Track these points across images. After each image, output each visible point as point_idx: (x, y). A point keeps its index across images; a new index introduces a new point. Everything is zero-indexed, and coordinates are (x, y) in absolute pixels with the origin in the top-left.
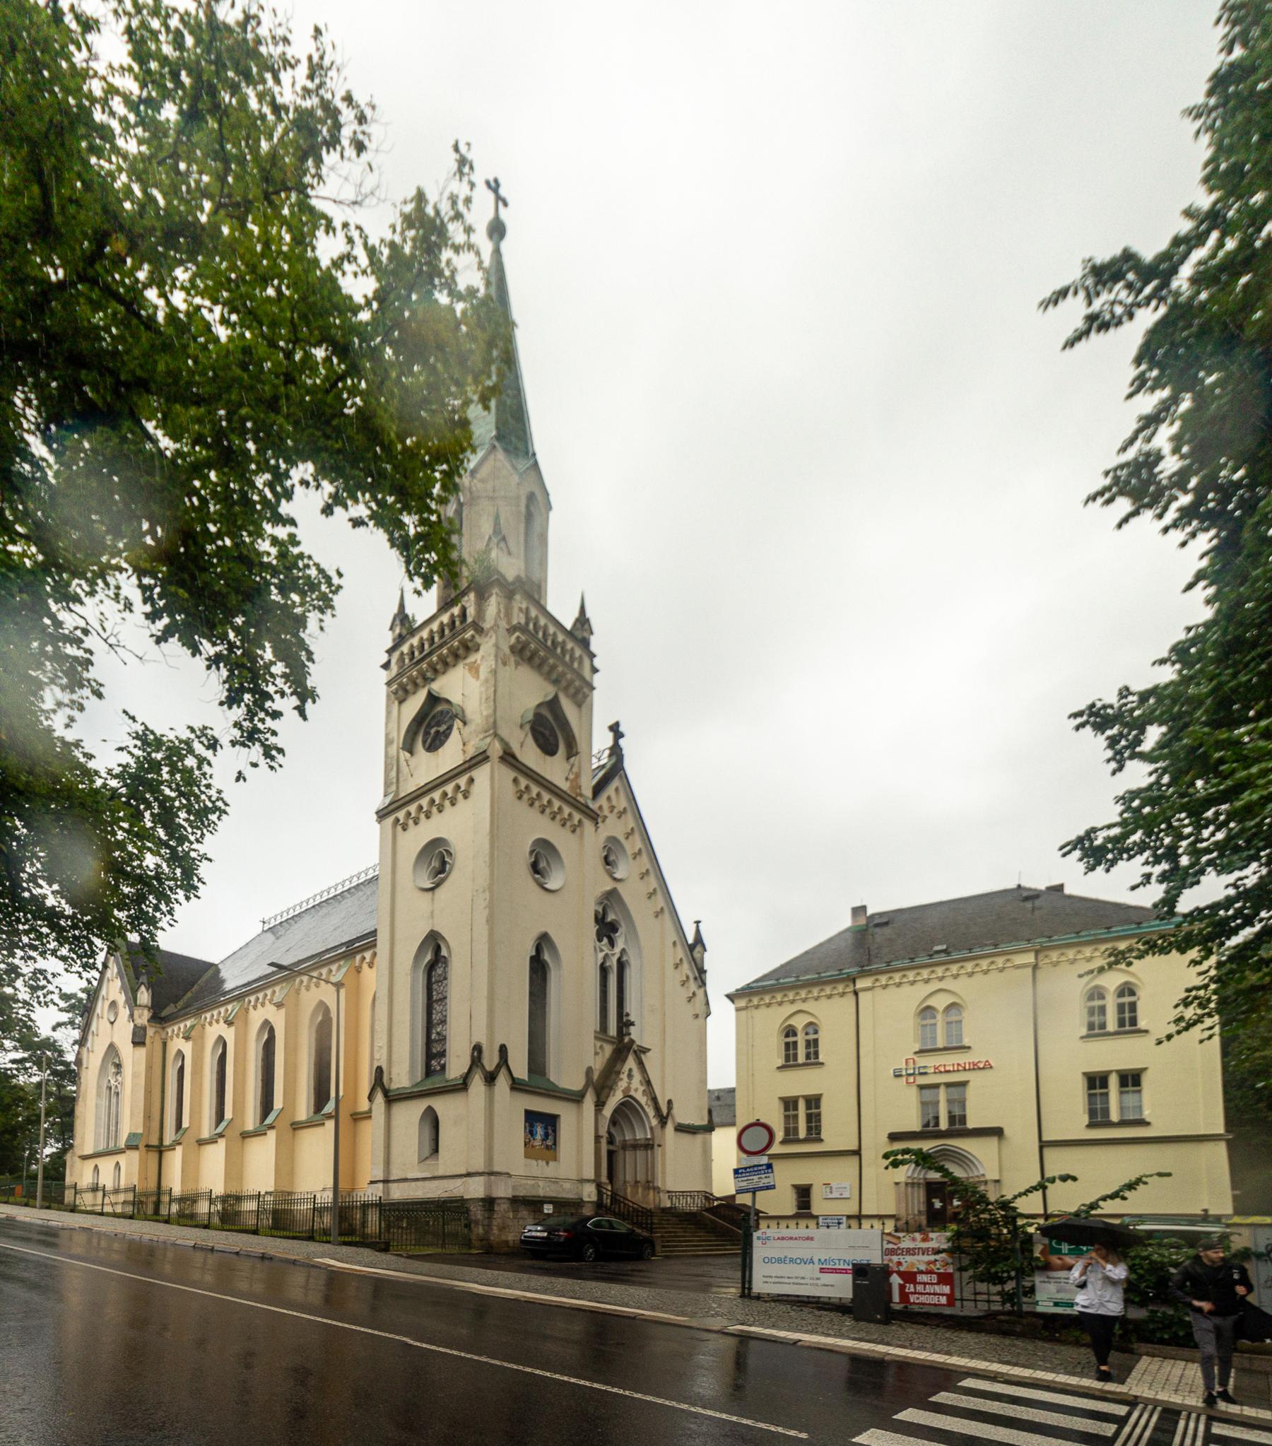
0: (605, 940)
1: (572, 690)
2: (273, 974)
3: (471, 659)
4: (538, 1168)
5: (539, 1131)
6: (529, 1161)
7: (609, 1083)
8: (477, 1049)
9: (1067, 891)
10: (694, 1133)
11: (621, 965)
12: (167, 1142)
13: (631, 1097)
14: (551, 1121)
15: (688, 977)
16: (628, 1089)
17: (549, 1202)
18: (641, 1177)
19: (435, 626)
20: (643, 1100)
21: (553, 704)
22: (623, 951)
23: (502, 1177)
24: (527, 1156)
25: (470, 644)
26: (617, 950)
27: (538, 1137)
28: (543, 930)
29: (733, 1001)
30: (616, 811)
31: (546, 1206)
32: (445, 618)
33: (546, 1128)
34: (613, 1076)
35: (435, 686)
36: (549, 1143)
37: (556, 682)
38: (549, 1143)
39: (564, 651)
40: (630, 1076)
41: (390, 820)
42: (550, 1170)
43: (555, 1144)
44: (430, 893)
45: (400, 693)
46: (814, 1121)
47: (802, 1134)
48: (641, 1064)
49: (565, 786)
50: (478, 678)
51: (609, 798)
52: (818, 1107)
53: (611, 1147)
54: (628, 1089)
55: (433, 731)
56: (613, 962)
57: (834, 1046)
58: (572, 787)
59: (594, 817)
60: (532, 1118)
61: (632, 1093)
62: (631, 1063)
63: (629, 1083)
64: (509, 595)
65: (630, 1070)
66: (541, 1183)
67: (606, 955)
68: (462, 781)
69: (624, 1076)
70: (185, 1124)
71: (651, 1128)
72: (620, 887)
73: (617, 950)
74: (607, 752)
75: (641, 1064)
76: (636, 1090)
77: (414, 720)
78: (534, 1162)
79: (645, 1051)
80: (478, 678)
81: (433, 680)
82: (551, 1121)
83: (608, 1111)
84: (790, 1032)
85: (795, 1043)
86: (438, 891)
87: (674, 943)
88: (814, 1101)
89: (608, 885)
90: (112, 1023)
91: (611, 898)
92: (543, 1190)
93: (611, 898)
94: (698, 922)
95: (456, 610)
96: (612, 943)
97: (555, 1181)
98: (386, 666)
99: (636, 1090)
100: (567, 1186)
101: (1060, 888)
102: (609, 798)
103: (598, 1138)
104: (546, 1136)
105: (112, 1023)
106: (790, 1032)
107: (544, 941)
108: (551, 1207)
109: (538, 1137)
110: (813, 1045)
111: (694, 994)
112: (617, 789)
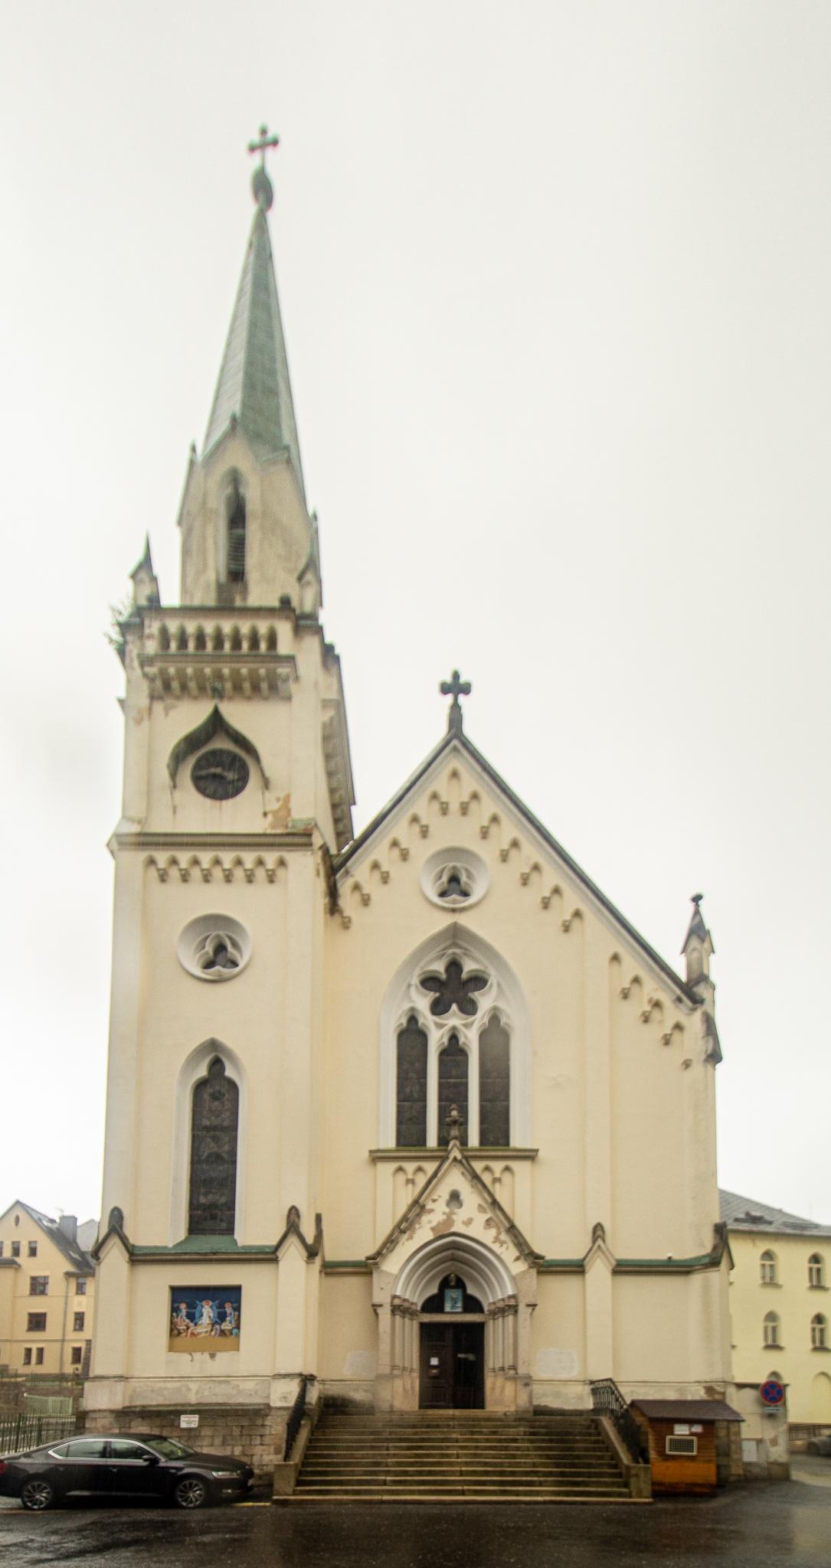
2: (439, 1168)
6: (174, 1355)
8: (293, 1213)
9: (123, 695)
10: (688, 1273)
17: (192, 1412)
18: (509, 1362)
20: (487, 1236)
23: (105, 1383)
27: (205, 1320)
33: (221, 1306)
42: (223, 1363)
43: (238, 1327)
71: (513, 1279)
94: (697, 899)
100: (250, 1385)
101: (121, 702)
104: (222, 1317)
107: (216, 1056)
109: (205, 1320)
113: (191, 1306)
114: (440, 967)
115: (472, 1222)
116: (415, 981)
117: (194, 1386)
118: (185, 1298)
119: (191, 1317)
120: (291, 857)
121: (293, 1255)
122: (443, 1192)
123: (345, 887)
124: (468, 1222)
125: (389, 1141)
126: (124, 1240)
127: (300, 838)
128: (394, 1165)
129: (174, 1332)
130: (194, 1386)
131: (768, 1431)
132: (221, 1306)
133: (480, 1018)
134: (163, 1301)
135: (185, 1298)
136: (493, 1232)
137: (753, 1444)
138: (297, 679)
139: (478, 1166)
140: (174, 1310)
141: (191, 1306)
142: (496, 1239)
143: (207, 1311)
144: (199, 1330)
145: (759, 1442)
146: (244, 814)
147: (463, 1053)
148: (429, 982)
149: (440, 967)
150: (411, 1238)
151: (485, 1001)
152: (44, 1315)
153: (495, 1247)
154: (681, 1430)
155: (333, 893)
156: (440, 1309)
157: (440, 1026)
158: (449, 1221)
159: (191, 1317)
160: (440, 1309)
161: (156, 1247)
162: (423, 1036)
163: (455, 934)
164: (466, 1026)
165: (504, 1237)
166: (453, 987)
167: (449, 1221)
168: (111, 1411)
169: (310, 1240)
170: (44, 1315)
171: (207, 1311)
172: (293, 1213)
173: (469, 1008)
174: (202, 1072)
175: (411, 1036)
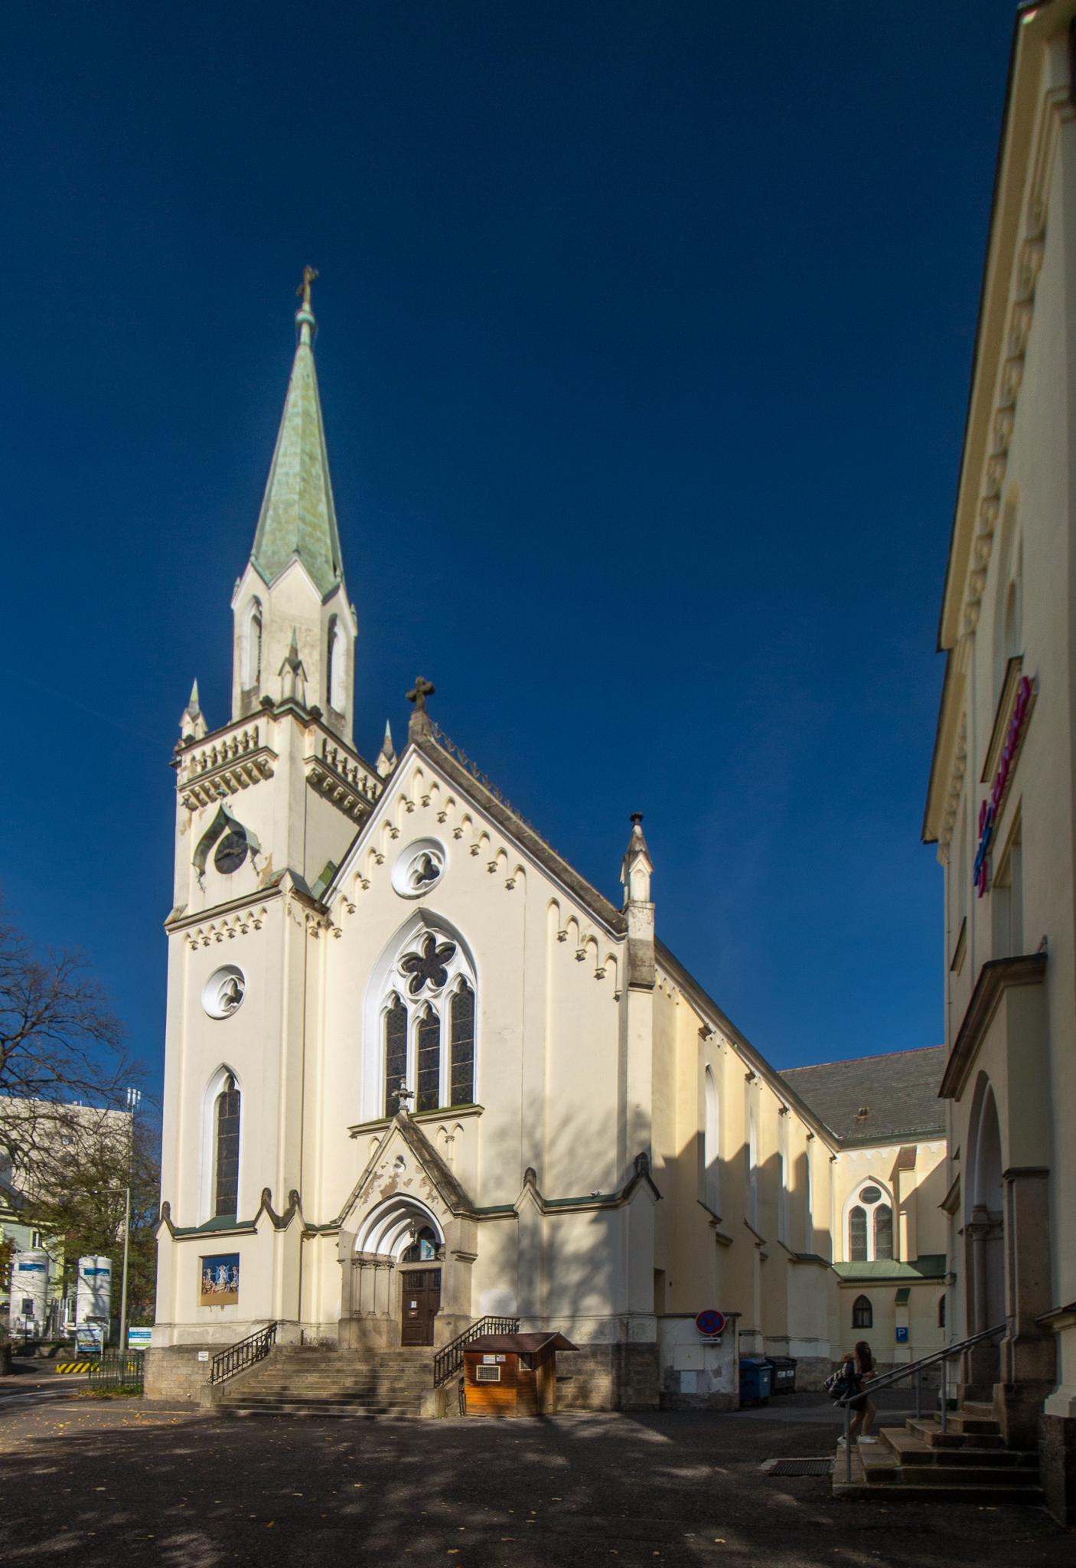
27: (221, 1281)
42: (228, 1313)
104: (231, 1277)
109: (221, 1281)
113: (214, 1271)
114: (418, 948)
115: (417, 1186)
116: (397, 965)
117: (211, 1330)
118: (211, 1263)
119: (213, 1278)
120: (269, 904)
121: (265, 1223)
122: (389, 1157)
123: (334, 903)
124: (410, 1180)
125: (376, 1110)
126: (170, 1225)
127: (271, 889)
128: (371, 1136)
129: (205, 1291)
130: (211, 1330)
131: (709, 1360)
132: (230, 1270)
133: (452, 986)
134: (197, 1266)
135: (211, 1263)
136: (427, 1189)
137: (693, 1376)
138: (275, 756)
139: (429, 1131)
140: (205, 1274)
141: (214, 1271)
142: (430, 1196)
143: (223, 1273)
144: (218, 1288)
145: (701, 1373)
146: (246, 880)
147: (437, 1020)
148: (411, 963)
149: (418, 948)
150: (366, 1201)
151: (456, 966)
152: (237, 1255)
153: (428, 1202)
154: (489, 1359)
155: (324, 911)
156: (417, 1259)
157: (416, 1002)
158: (393, 1184)
159: (213, 1278)
160: (417, 1259)
161: (343, 1298)
162: (405, 1010)
163: (426, 917)
164: (435, 997)
165: (435, 1193)
166: (426, 967)
167: (393, 1184)
168: (163, 1348)
169: (280, 1213)
170: (237, 1255)
171: (223, 1273)
172: (267, 1193)
173: (441, 979)
174: (221, 1087)
175: (396, 1018)
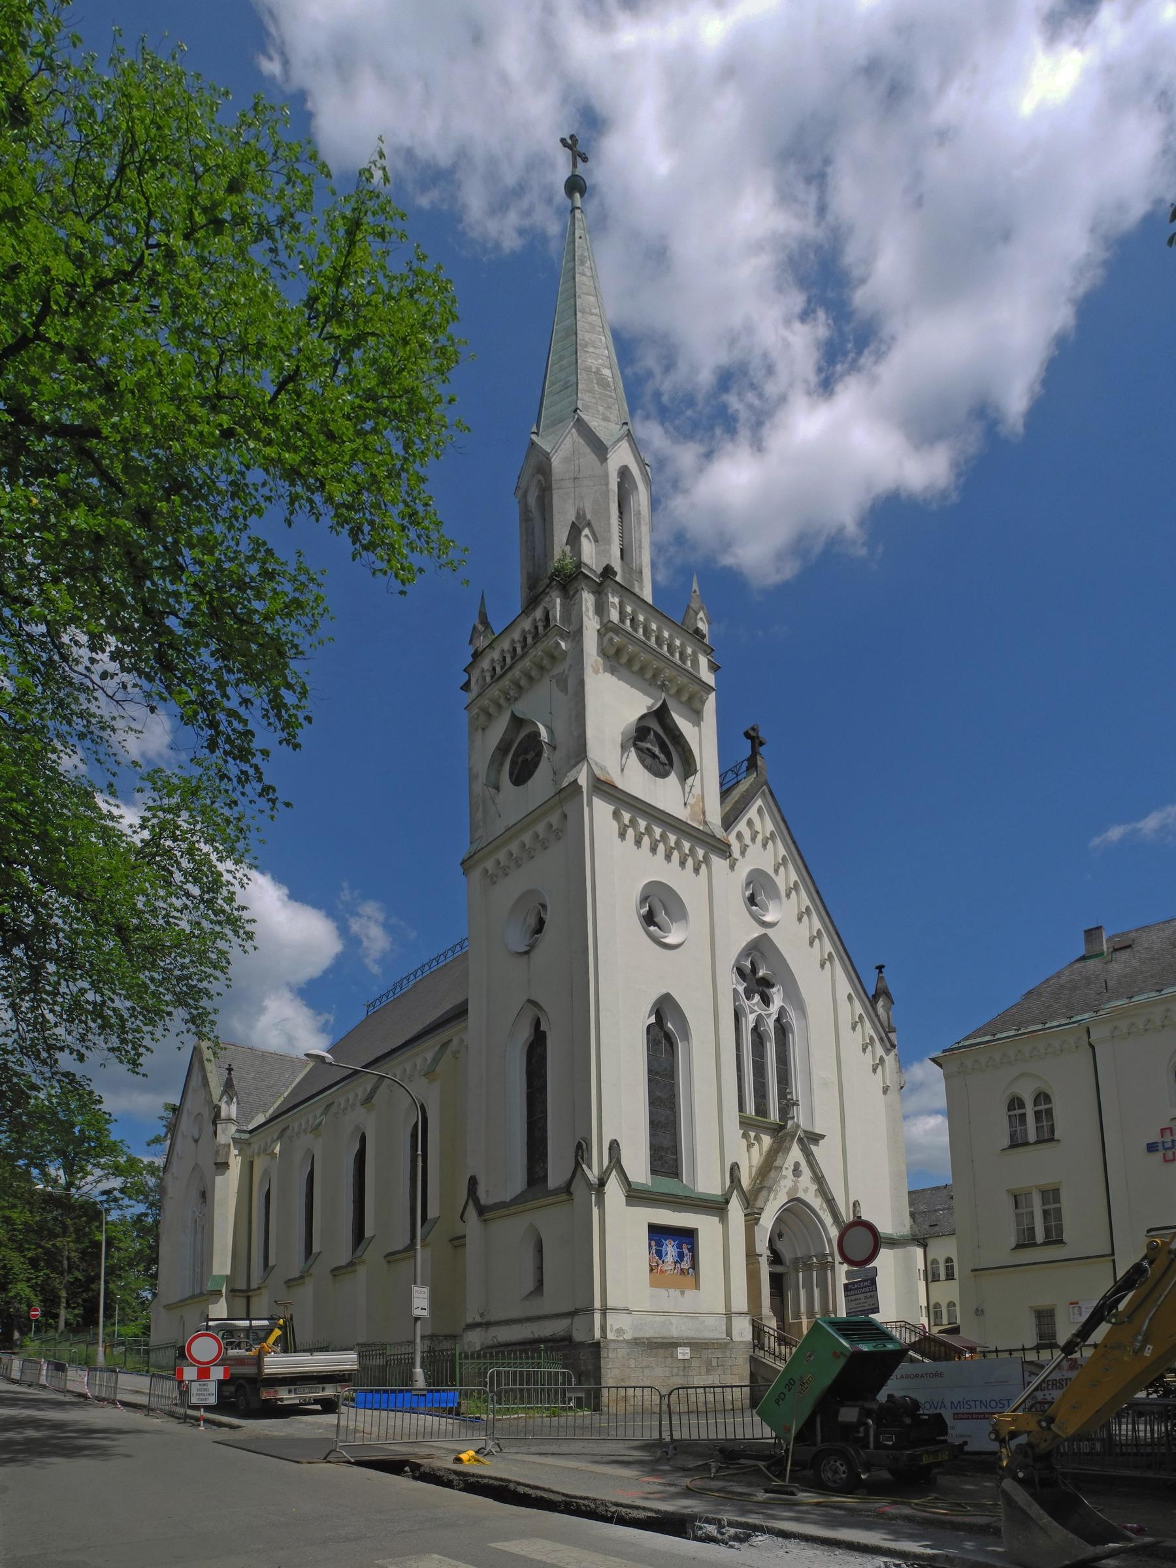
0: (757, 998)
1: (684, 698)
3: (558, 670)
4: (669, 1299)
5: (670, 1249)
7: (767, 1183)
11: (782, 1029)
12: (254, 1285)
13: (798, 1200)
14: (687, 1237)
15: (871, 1038)
16: (795, 1188)
17: (685, 1345)
19: (516, 635)
20: (817, 1203)
21: (661, 714)
22: (782, 1011)
24: (654, 1284)
25: (556, 654)
26: (774, 1009)
28: (665, 991)
29: (940, 1065)
30: (760, 838)
31: (680, 1350)
32: (527, 624)
33: (679, 1247)
34: (773, 1174)
35: (522, 708)
36: (685, 1265)
37: (663, 687)
38: (685, 1265)
39: (671, 648)
40: (797, 1171)
41: (476, 874)
42: (689, 1300)
44: (526, 957)
45: (482, 718)
46: (1052, 1216)
47: (1040, 1236)
48: (809, 1155)
49: (682, 814)
50: (567, 693)
51: (750, 823)
52: (1057, 1199)
53: (779, 1269)
54: (795, 1188)
55: (520, 759)
56: (770, 1025)
57: (1070, 1115)
58: (693, 815)
59: (724, 850)
60: (657, 1232)
61: (801, 1195)
62: (795, 1153)
63: (796, 1182)
64: (599, 591)
65: (797, 1165)
66: (674, 1320)
67: (760, 1016)
68: (554, 819)
69: (788, 1172)
70: (316, 1249)
72: (770, 932)
73: (774, 1009)
74: (746, 764)
75: (809, 1155)
76: (806, 1190)
77: (498, 748)
78: (663, 1292)
79: (816, 1138)
80: (567, 693)
81: (516, 699)
82: (687, 1237)
83: (767, 1221)
84: (1015, 1103)
85: (1024, 1114)
86: (532, 954)
87: (850, 997)
88: (1051, 1195)
89: (757, 932)
90: (196, 1141)
91: (760, 949)
92: (678, 1328)
93: (760, 949)
95: (538, 614)
96: (766, 1000)
97: (694, 1315)
98: (466, 687)
99: (806, 1190)
102: (750, 823)
103: (752, 1255)
104: (681, 1256)
105: (196, 1141)
106: (1015, 1103)
108: (687, 1350)
110: (1045, 1116)
111: (882, 1059)
112: (760, 811)
